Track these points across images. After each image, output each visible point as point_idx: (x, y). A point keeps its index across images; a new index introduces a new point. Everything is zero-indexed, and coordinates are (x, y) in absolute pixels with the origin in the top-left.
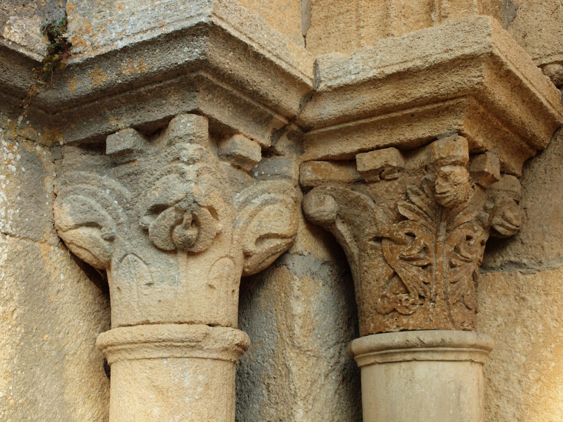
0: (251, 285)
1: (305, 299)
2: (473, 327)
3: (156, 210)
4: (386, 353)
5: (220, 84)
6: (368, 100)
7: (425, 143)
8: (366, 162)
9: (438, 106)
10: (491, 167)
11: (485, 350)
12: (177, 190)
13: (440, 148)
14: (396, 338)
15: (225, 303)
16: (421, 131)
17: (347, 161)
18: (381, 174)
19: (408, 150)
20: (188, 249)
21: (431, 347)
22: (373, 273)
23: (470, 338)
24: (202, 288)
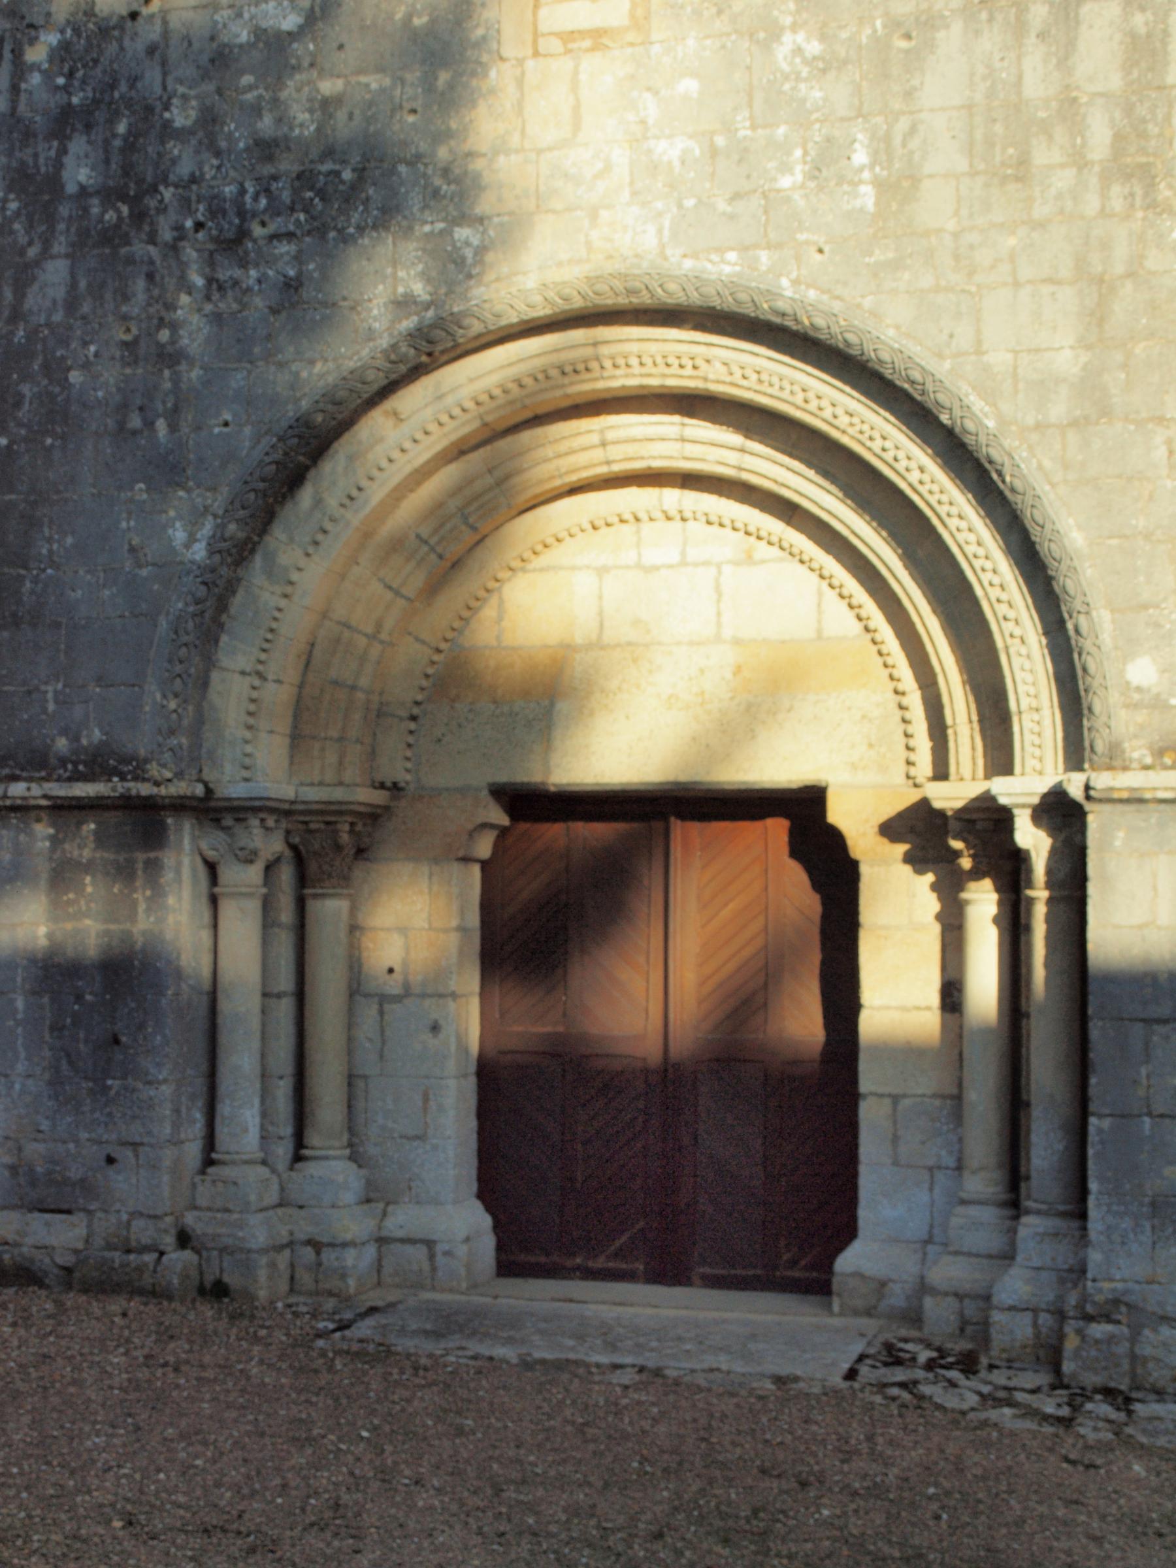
0: (268, 868)
1: (286, 875)
2: (347, 887)
3: (242, 849)
4: (315, 896)
5: (463, 1298)
6: (315, 807)
7: (335, 823)
8: (313, 826)
9: (341, 813)
10: (359, 828)
11: (350, 895)
12: (252, 845)
13: (339, 826)
14: (320, 891)
15: (261, 874)
16: (333, 819)
17: (306, 823)
18: (317, 831)
19: (328, 823)
20: (251, 862)
21: (510, 365)
22: (312, 867)
23: (345, 891)
24: (253, 874)
